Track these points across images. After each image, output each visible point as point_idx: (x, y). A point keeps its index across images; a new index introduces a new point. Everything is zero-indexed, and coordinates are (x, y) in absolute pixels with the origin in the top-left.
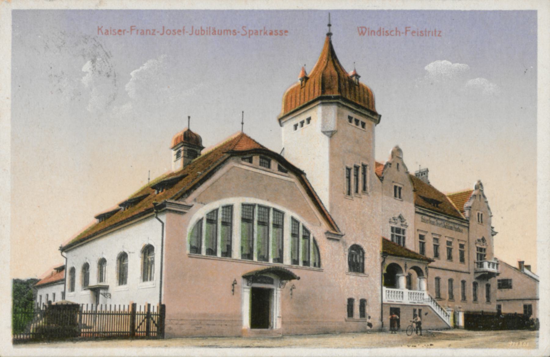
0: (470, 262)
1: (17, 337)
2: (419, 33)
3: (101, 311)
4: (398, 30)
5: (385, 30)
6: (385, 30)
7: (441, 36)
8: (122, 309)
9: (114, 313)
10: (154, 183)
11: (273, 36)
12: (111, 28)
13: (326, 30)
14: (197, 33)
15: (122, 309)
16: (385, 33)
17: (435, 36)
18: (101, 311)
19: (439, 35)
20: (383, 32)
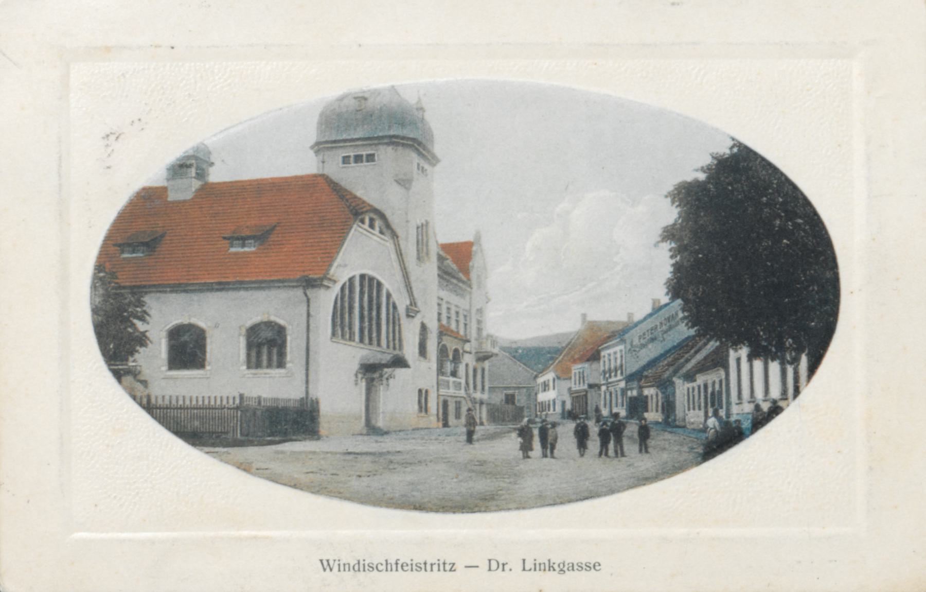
0: (387, 352)
1: (632, 393)
2: (414, 567)
3: (184, 405)
4: (389, 562)
5: (366, 563)
6: (366, 563)
7: (455, 570)
8: (206, 402)
9: (182, 406)
10: (167, 341)
11: (576, 573)
12: (412, 560)
13: (534, 562)
14: (347, 567)
15: (206, 402)
16: (367, 567)
17: (445, 570)
18: (184, 405)
19: (451, 570)
20: (364, 565)
